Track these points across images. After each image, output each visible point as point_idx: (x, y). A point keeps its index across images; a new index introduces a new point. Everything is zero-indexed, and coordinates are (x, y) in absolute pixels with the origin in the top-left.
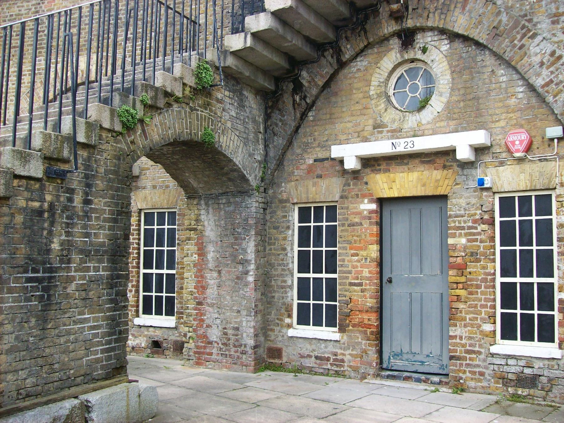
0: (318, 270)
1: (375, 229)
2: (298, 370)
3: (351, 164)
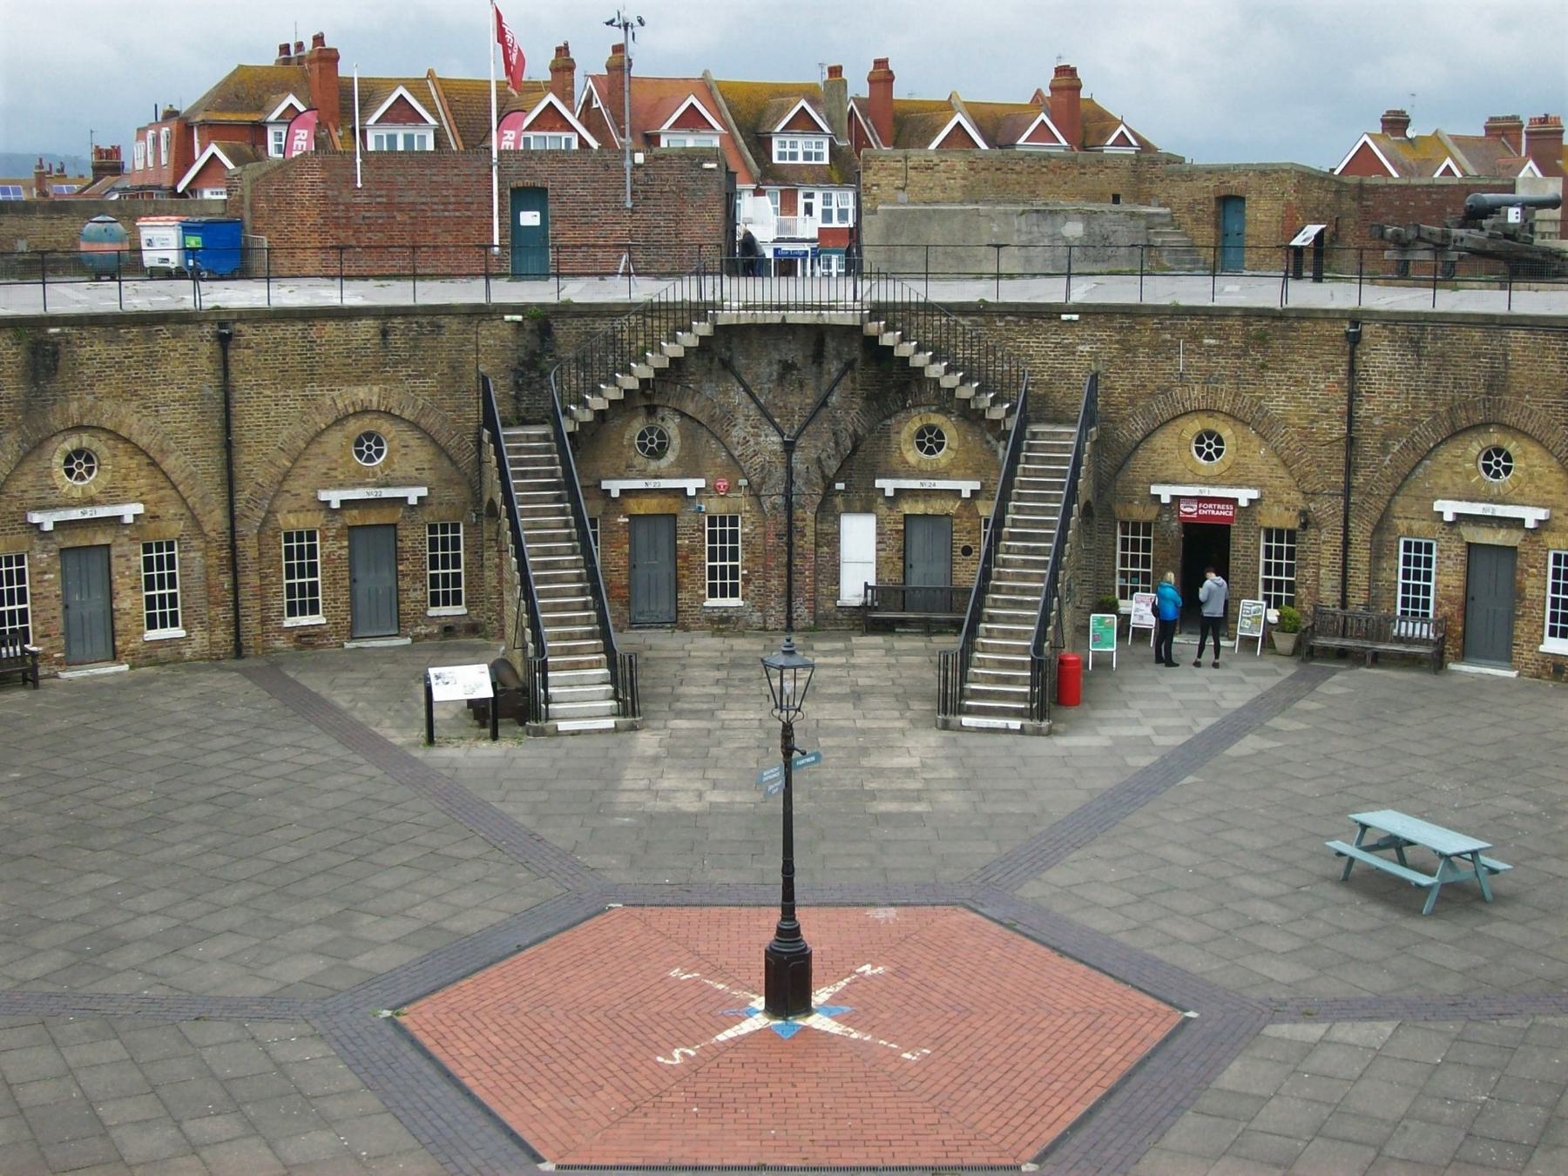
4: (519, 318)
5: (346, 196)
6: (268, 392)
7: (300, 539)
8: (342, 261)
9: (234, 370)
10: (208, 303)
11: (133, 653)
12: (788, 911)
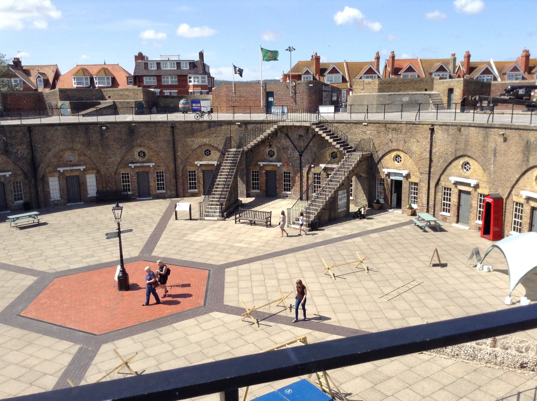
3: (261, 165)
5: (231, 95)
8: (234, 109)
9: (175, 134)
10: (170, 119)
11: (154, 195)
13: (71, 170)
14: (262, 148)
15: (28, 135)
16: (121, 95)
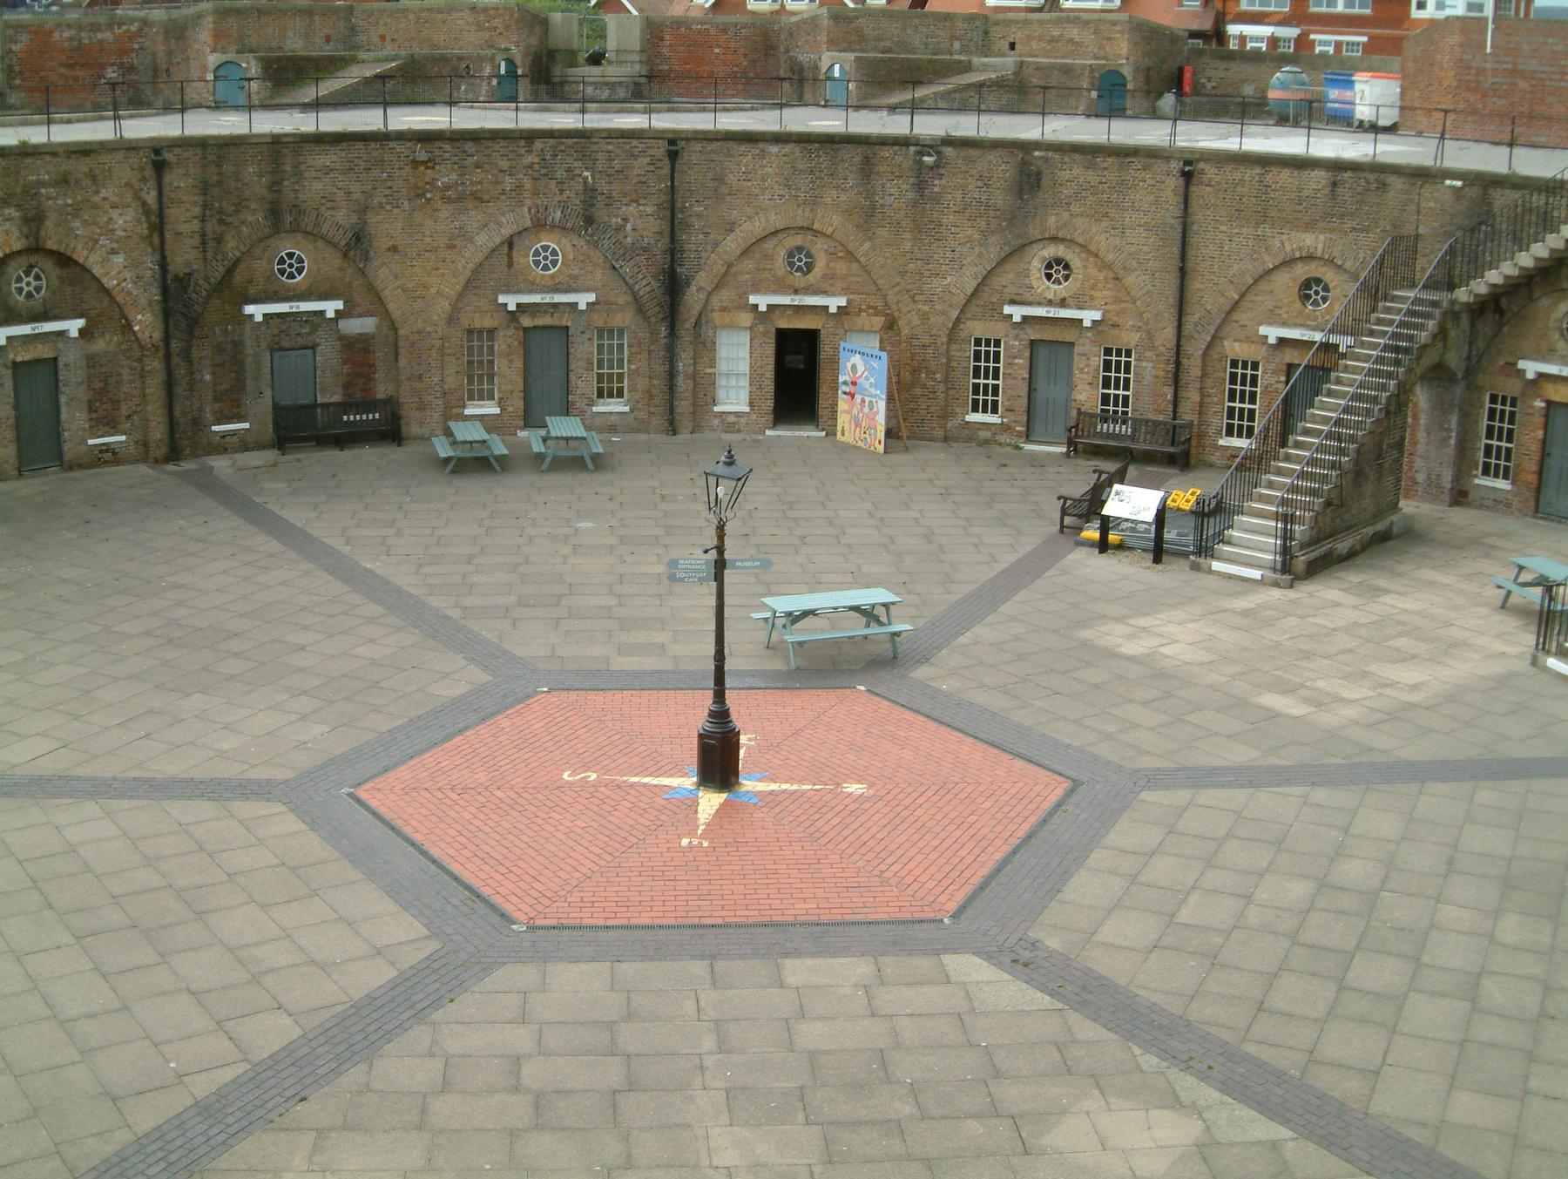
0: (1499, 439)
1: (1542, 420)
2: (1480, 507)
4: (1459, 183)
6: (1223, 228)
7: (1245, 367)
9: (1194, 202)
10: (1182, 143)
12: (720, 696)
13: (799, 309)
14: (1545, 302)
15: (666, 171)
16: (1053, 40)
